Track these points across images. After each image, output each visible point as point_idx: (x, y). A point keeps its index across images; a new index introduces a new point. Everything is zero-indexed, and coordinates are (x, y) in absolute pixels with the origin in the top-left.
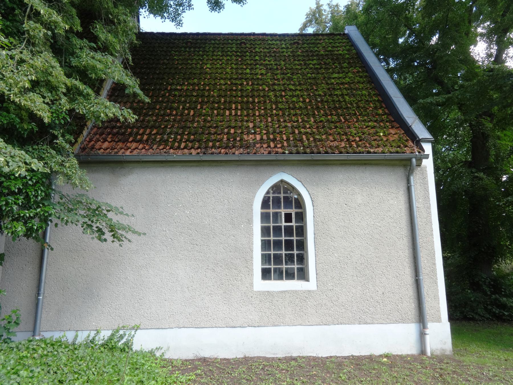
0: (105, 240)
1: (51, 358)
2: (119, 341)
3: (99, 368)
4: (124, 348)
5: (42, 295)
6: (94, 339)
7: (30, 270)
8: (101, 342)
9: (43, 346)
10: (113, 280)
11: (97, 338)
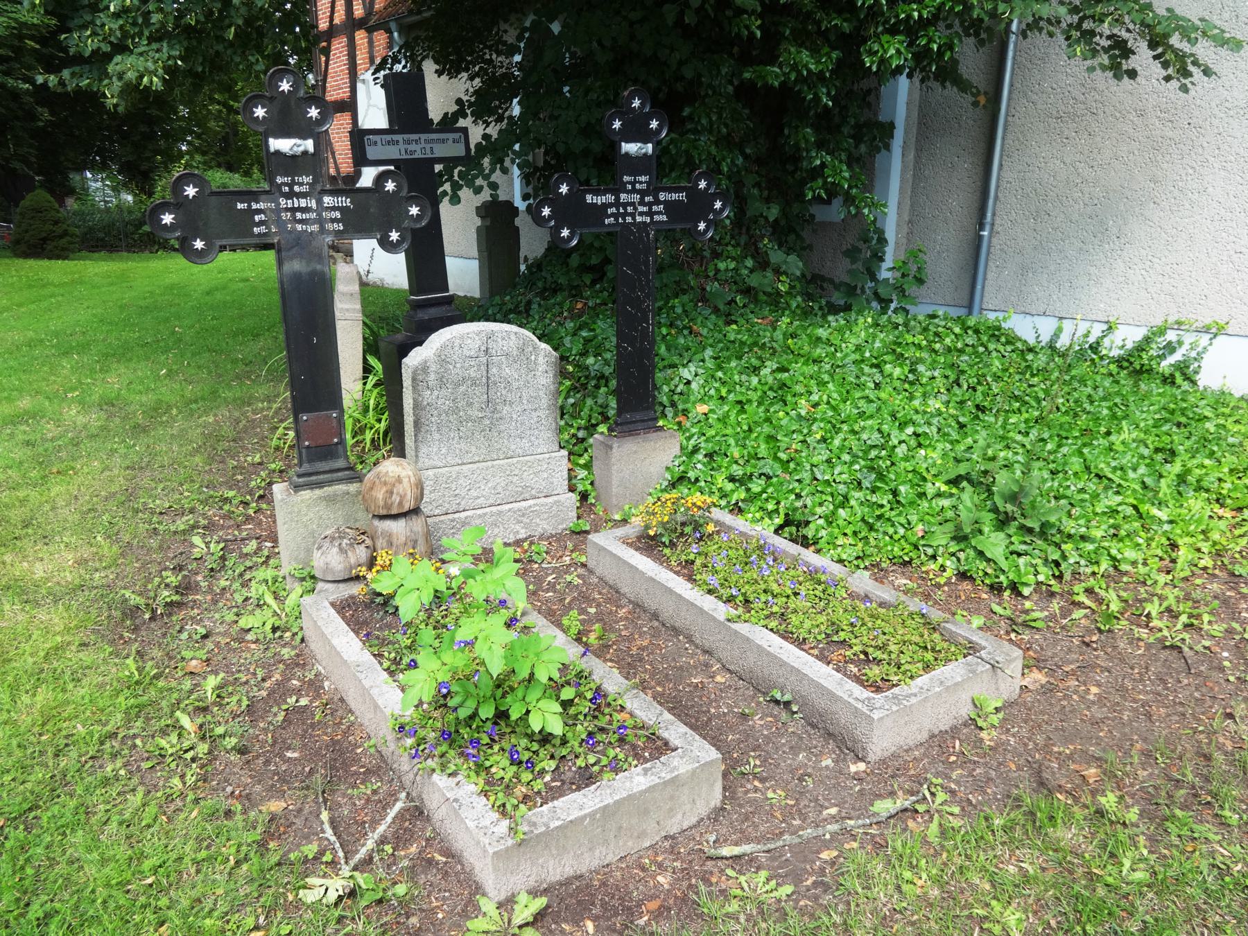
0: (1132, 74)
1: (967, 358)
2: (1162, 357)
3: (1076, 402)
4: (1172, 376)
5: (988, 227)
6: (1098, 343)
7: (966, 167)
8: (1115, 353)
9: (957, 330)
10: (1164, 197)
11: (1106, 342)
